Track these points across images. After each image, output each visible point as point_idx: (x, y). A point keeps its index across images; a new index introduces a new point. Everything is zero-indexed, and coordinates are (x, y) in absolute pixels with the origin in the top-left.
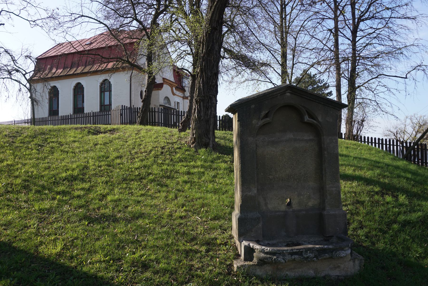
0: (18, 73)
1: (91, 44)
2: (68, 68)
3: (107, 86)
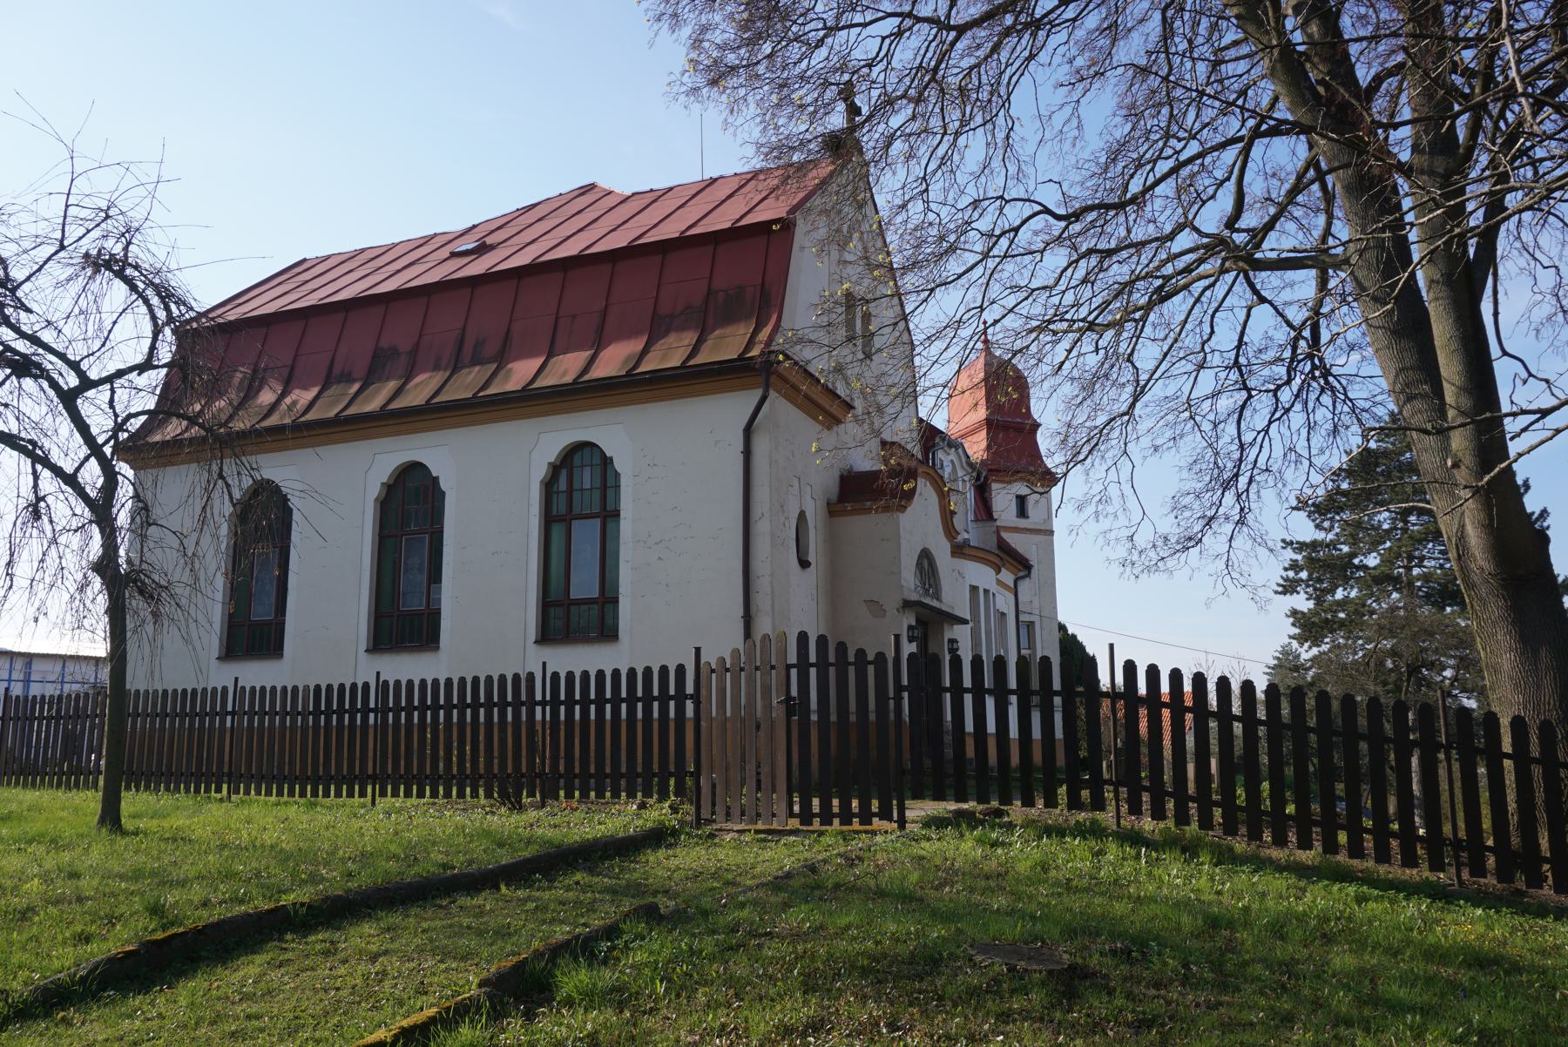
0: (28, 383)
1: (482, 249)
2: (347, 378)
3: (586, 478)
